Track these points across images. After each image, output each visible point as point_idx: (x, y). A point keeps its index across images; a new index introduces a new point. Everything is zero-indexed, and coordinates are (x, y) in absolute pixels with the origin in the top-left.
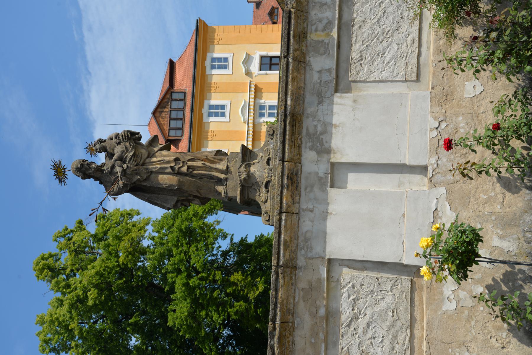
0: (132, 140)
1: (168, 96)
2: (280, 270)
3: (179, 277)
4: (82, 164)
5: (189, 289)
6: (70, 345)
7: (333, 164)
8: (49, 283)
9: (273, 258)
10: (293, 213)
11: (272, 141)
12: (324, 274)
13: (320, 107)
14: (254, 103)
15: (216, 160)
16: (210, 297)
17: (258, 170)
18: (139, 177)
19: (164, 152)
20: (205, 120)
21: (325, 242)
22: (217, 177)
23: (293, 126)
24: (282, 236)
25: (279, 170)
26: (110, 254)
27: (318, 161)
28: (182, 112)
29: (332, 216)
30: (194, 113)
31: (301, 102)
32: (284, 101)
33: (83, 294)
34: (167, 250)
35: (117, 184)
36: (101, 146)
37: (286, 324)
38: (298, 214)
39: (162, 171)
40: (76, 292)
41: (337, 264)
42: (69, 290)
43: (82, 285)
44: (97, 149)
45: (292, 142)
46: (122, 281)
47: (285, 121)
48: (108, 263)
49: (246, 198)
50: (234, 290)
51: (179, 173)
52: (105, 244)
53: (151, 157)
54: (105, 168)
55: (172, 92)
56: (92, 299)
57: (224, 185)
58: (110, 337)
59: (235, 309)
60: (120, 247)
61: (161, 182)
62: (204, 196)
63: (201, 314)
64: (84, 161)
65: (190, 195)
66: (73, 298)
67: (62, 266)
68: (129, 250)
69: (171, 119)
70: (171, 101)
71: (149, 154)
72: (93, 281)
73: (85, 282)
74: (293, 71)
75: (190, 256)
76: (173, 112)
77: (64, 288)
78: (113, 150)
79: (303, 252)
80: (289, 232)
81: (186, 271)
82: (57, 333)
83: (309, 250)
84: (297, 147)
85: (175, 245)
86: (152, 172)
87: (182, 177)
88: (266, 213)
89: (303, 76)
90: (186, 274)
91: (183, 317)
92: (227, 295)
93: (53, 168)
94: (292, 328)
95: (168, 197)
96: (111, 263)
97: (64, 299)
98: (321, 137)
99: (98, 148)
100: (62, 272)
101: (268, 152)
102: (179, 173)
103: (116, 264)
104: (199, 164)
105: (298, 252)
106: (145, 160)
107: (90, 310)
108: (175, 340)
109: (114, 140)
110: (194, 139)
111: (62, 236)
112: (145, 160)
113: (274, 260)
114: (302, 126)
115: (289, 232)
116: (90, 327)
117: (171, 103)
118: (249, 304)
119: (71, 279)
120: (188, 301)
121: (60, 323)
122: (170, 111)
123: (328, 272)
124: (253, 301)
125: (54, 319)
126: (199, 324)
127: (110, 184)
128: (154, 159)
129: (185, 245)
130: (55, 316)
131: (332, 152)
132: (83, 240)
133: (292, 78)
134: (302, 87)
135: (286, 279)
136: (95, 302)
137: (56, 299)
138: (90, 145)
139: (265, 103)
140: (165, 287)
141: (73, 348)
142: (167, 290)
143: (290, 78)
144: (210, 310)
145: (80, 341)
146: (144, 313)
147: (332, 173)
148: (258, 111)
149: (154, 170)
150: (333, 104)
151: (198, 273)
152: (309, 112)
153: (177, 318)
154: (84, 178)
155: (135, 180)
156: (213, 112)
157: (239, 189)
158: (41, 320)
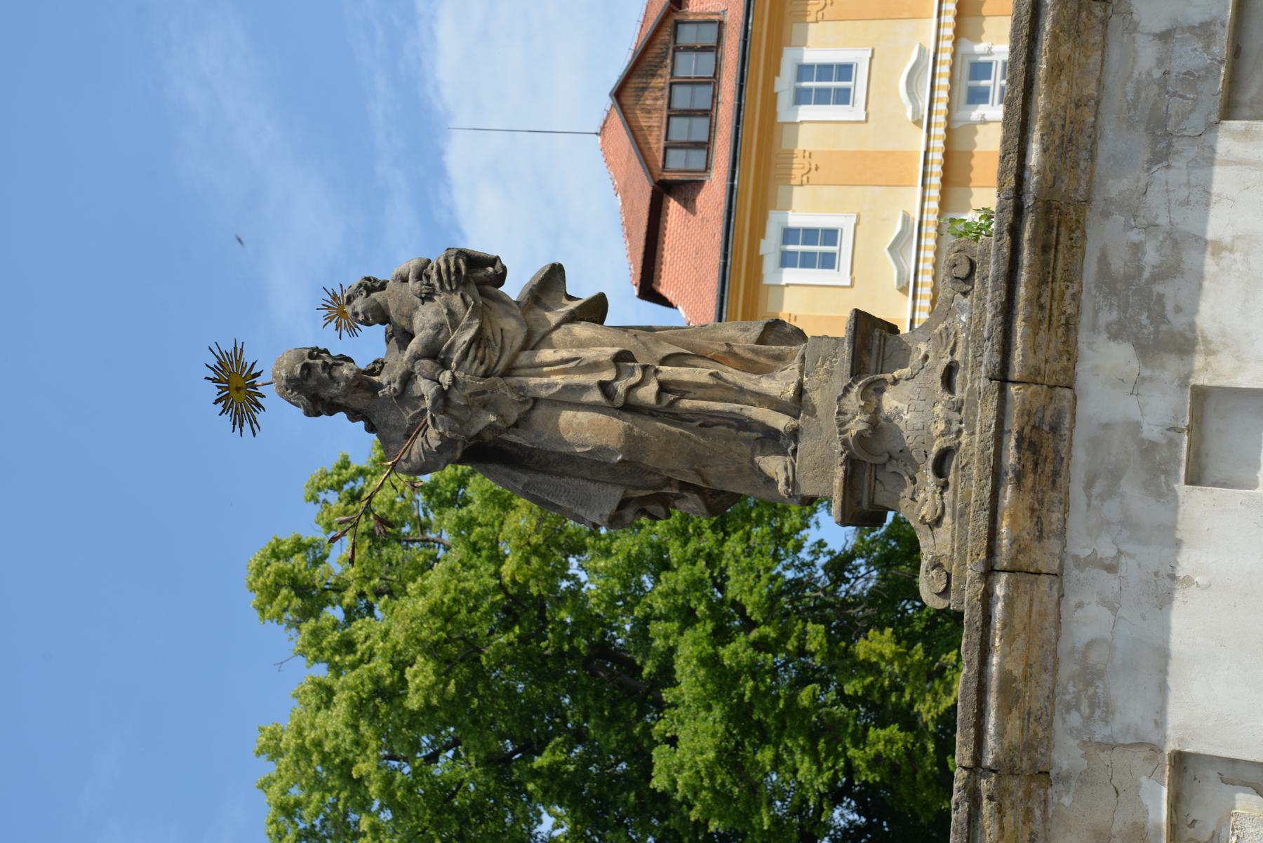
0: (473, 288)
1: (665, 36)
2: (984, 785)
3: (689, 633)
4: (306, 367)
5: (721, 678)
6: (357, 823)
7: (1201, 395)
8: (294, 630)
9: (958, 737)
10: (1039, 573)
11: (967, 301)
12: (1159, 808)
13: (1160, 174)
14: (954, 56)
15: (763, 360)
16: (787, 706)
17: (909, 405)
18: (492, 418)
19: (582, 330)
20: (783, 114)
21: (1163, 688)
22: (763, 424)
23: (1045, 248)
24: (995, 660)
25: (986, 414)
26: (475, 548)
27: (1140, 380)
28: (711, 89)
29: (1193, 589)
30: (746, 91)
31: (1084, 154)
32: (1014, 155)
33: (392, 671)
34: (651, 546)
35: (420, 439)
36: (368, 303)
38: (1057, 575)
39: (570, 398)
40: (372, 665)
41: (1213, 775)
42: (349, 658)
43: (388, 645)
44: (356, 314)
45: (1042, 307)
46: (511, 636)
47: (1015, 231)
48: (466, 580)
49: (865, 505)
50: (868, 689)
51: (630, 408)
52: (460, 519)
53: (536, 347)
54: (382, 379)
55: (677, 23)
56: (418, 690)
57: (785, 454)
58: (477, 808)
59: (870, 752)
60: (506, 528)
61: (568, 437)
62: (716, 484)
63: (759, 757)
64: (316, 353)
65: (668, 482)
66: (362, 684)
67: (332, 580)
68: (534, 540)
69: (673, 113)
70: (674, 51)
71: (529, 334)
72: (424, 634)
73: (398, 636)
74: (1055, 37)
75: (723, 571)
76: (678, 90)
77: (336, 651)
78: (410, 319)
79: (1075, 719)
80: (1019, 643)
81: (712, 618)
82: (319, 784)
83: (1098, 713)
84: (1061, 327)
85: (676, 530)
86: (536, 400)
87: (639, 420)
88: (937, 565)
89: (1096, 57)
90: (709, 626)
91: (701, 765)
92: (843, 698)
93: (212, 375)
95: (592, 487)
96: (480, 579)
97: (337, 685)
98: (1159, 288)
99: (359, 309)
100: (333, 596)
101: (947, 339)
102: (630, 408)
103: (493, 582)
104: (698, 374)
105: (1057, 718)
106: (515, 357)
107: (414, 720)
108: (676, 832)
109: (413, 285)
110: (746, 180)
111: (331, 487)
112: (515, 357)
113: (964, 744)
114: (1083, 248)
115: (1019, 643)
116: (416, 772)
117: (673, 60)
118: (917, 738)
119: (358, 623)
120: (717, 712)
121: (325, 758)
122: (671, 84)
123: (1176, 802)
124: (931, 727)
125: (307, 743)
126: (753, 788)
127: (398, 435)
128: (546, 355)
129: (708, 533)
130: (310, 735)
131: (1200, 347)
132: (393, 503)
133: (1051, 68)
134: (1090, 98)
135: (1009, 819)
136: (427, 699)
137: (313, 682)
138: (334, 297)
139: (990, 53)
140: (643, 663)
141: (364, 834)
142: (650, 673)
143: (1042, 66)
144: (786, 748)
145: (387, 815)
146: (579, 736)
147: (1197, 427)
148: (965, 83)
149: (544, 393)
150: (1211, 161)
151: (749, 625)
152: (1114, 194)
153: (681, 767)
154: (312, 412)
155: (481, 427)
156: (809, 90)
157: (839, 472)
158: (272, 743)
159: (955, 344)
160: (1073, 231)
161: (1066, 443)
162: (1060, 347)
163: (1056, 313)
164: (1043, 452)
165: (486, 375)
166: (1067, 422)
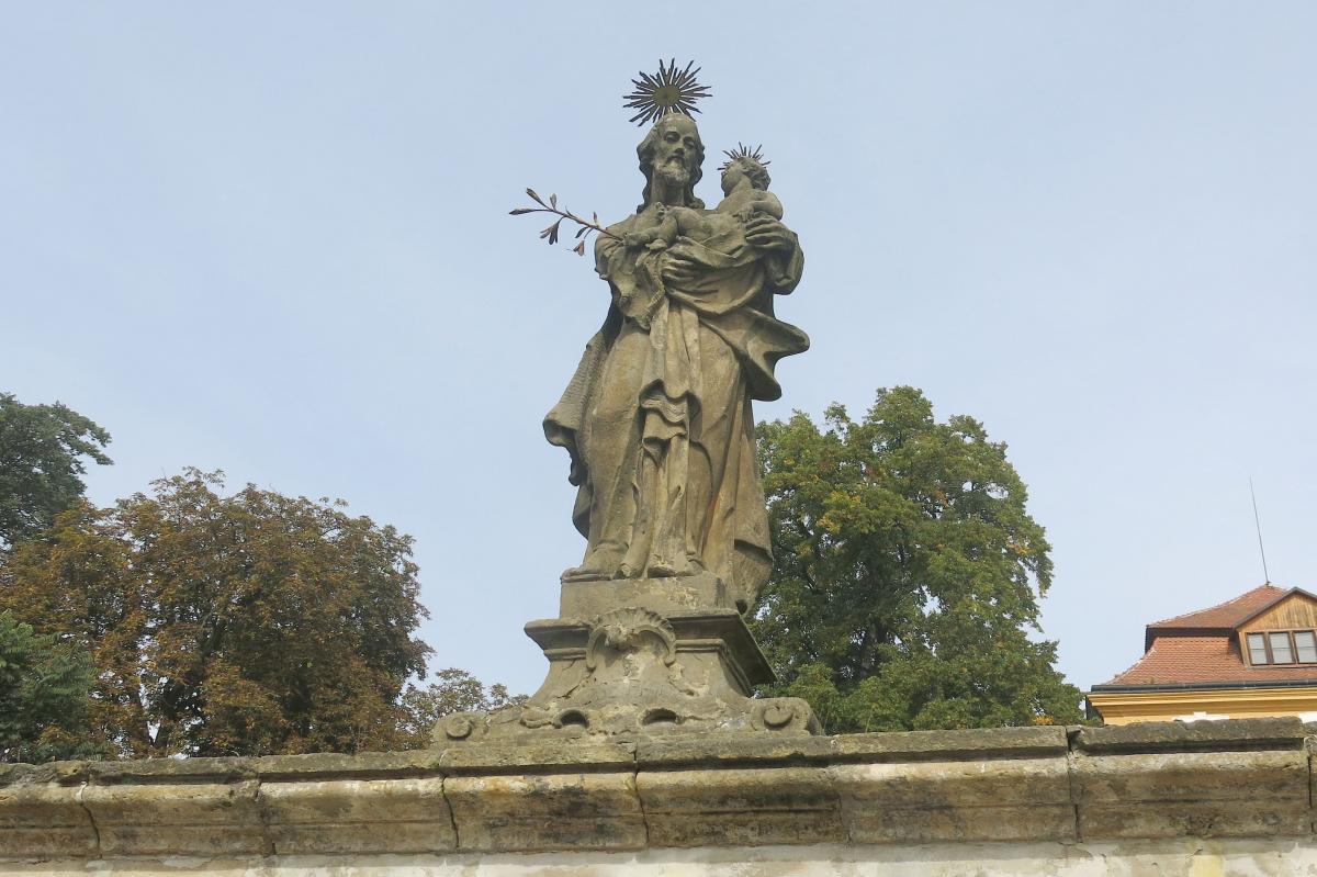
10: (455, 827)
31: (901, 832)
37: (89, 830)
45: (723, 802)
89: (1012, 832)
93: (667, 67)
94: (79, 851)
112: (690, 306)
135: (221, 816)
159: (700, 719)
160: (815, 828)
161: (589, 845)
162: (689, 829)
163: (721, 818)
164: (574, 821)
165: (666, 281)
166: (612, 844)
